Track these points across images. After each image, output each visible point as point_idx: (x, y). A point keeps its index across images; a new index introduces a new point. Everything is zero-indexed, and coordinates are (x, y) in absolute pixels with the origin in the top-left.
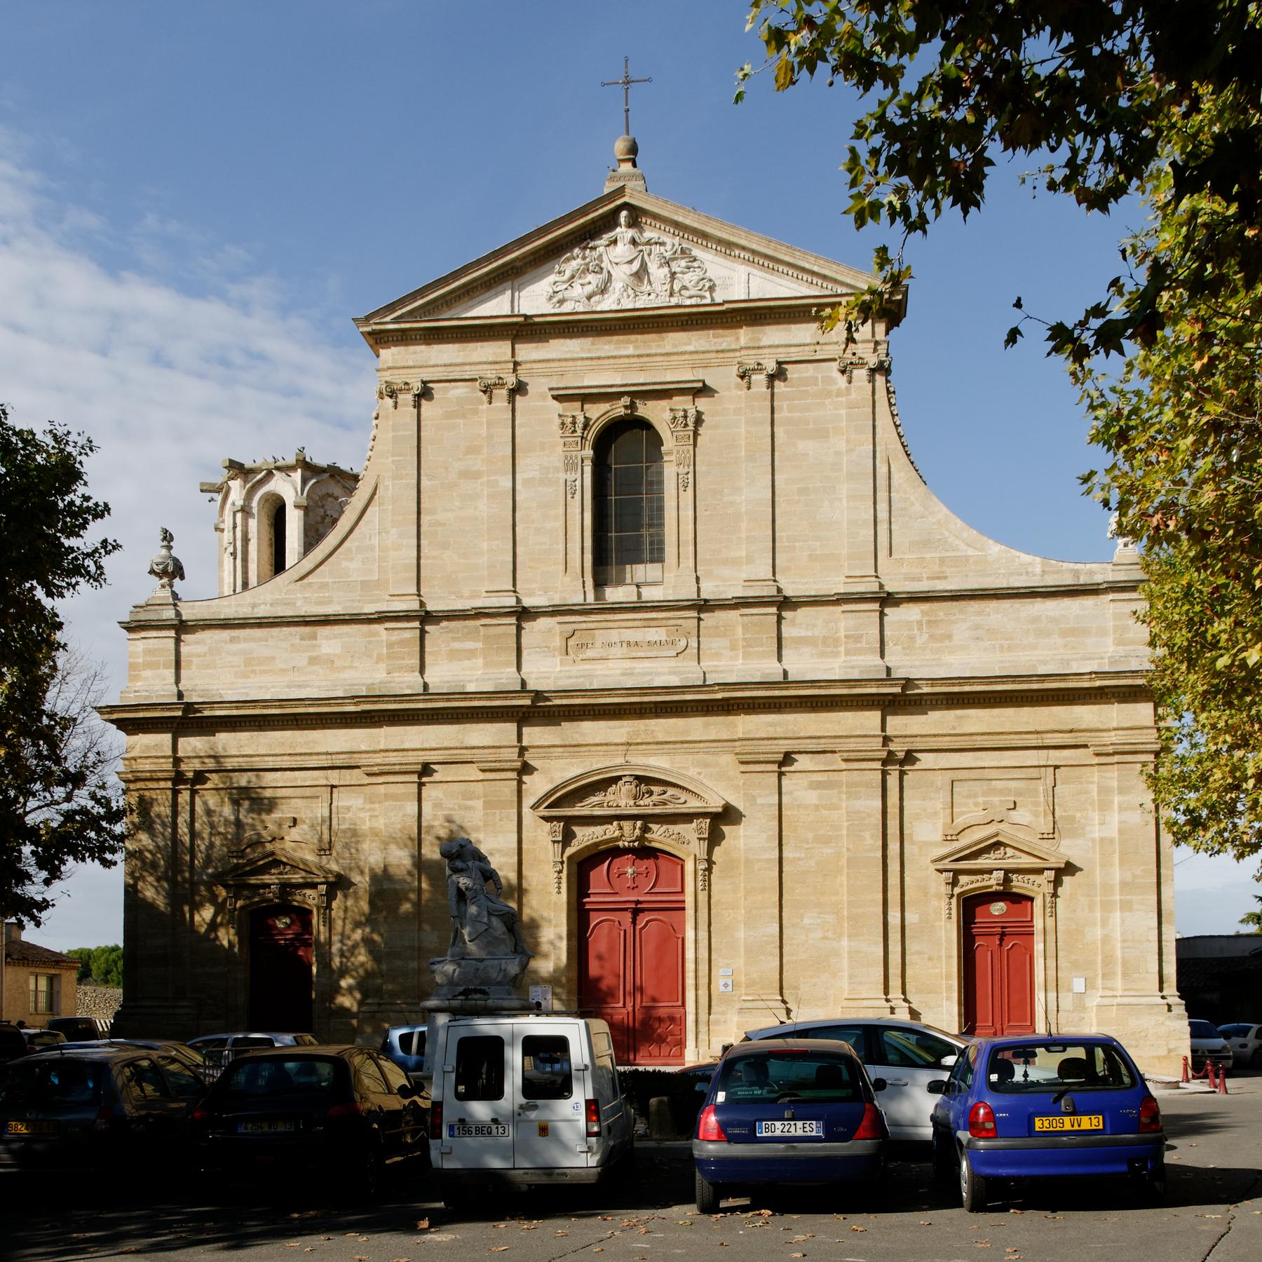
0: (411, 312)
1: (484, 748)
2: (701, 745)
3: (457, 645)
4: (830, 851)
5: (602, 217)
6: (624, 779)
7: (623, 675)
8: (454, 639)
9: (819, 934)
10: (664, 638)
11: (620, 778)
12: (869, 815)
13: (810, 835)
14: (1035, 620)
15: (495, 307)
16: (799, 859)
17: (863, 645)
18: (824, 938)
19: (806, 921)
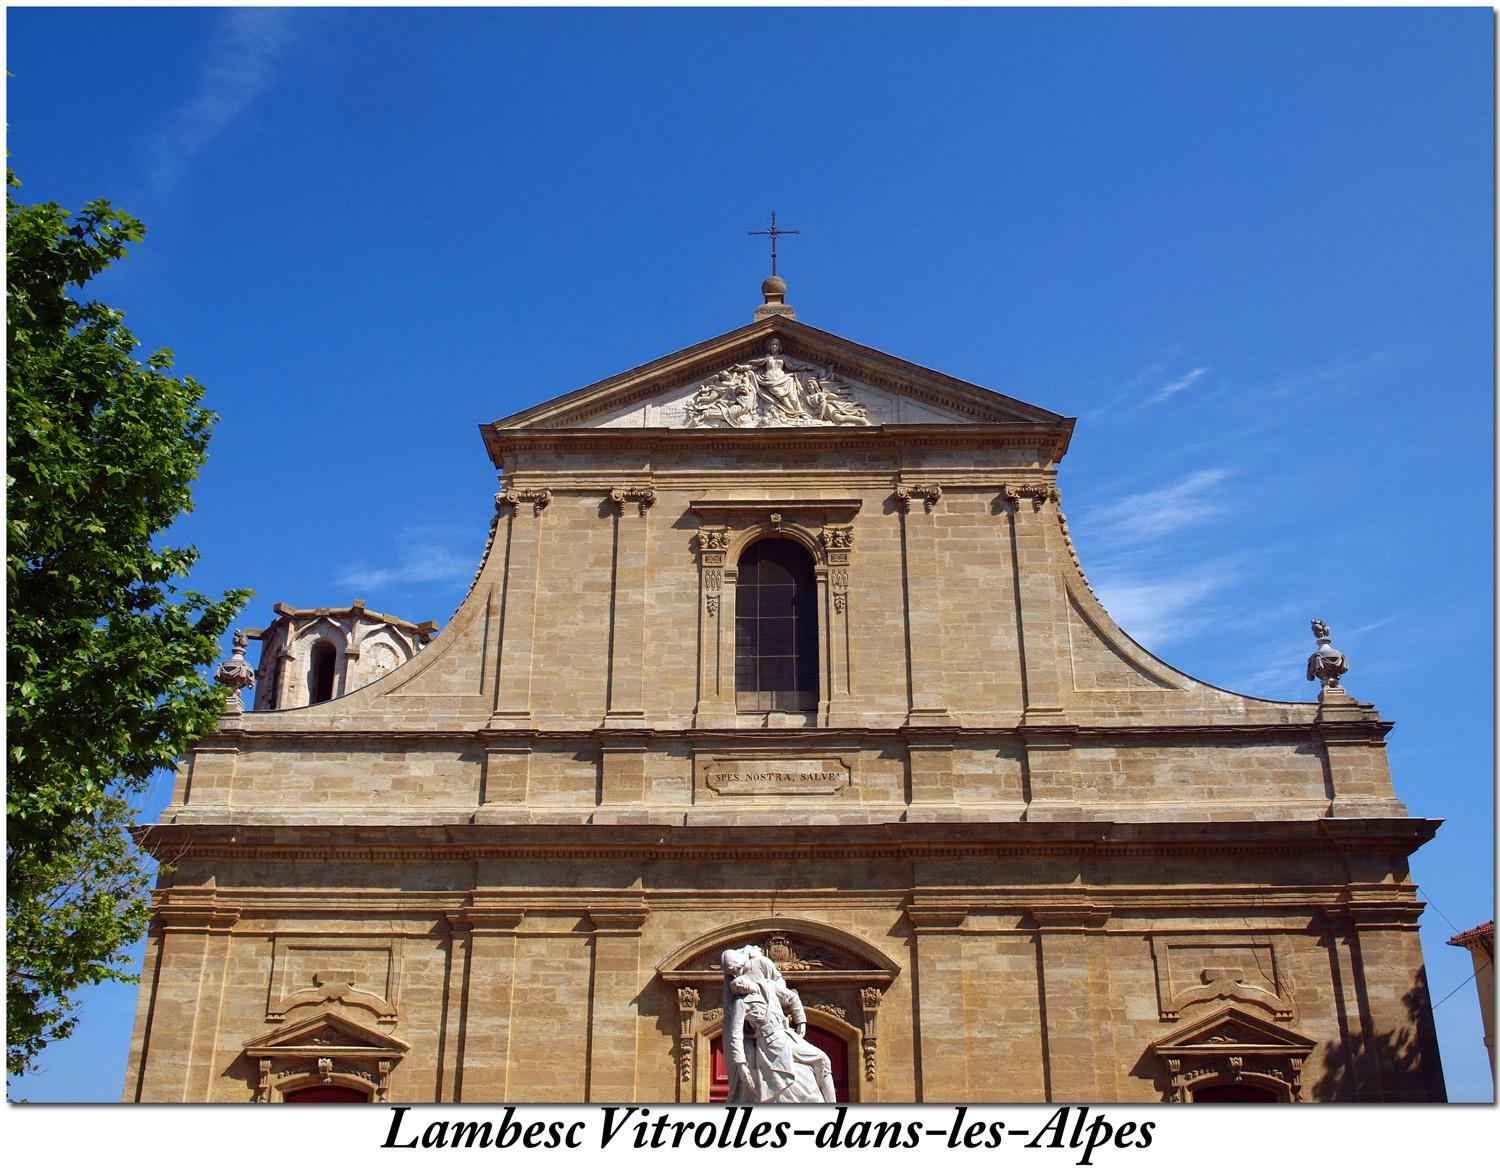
4: (1028, 1030)
8: (568, 765)
10: (820, 771)
13: (1002, 1011)
16: (990, 1040)
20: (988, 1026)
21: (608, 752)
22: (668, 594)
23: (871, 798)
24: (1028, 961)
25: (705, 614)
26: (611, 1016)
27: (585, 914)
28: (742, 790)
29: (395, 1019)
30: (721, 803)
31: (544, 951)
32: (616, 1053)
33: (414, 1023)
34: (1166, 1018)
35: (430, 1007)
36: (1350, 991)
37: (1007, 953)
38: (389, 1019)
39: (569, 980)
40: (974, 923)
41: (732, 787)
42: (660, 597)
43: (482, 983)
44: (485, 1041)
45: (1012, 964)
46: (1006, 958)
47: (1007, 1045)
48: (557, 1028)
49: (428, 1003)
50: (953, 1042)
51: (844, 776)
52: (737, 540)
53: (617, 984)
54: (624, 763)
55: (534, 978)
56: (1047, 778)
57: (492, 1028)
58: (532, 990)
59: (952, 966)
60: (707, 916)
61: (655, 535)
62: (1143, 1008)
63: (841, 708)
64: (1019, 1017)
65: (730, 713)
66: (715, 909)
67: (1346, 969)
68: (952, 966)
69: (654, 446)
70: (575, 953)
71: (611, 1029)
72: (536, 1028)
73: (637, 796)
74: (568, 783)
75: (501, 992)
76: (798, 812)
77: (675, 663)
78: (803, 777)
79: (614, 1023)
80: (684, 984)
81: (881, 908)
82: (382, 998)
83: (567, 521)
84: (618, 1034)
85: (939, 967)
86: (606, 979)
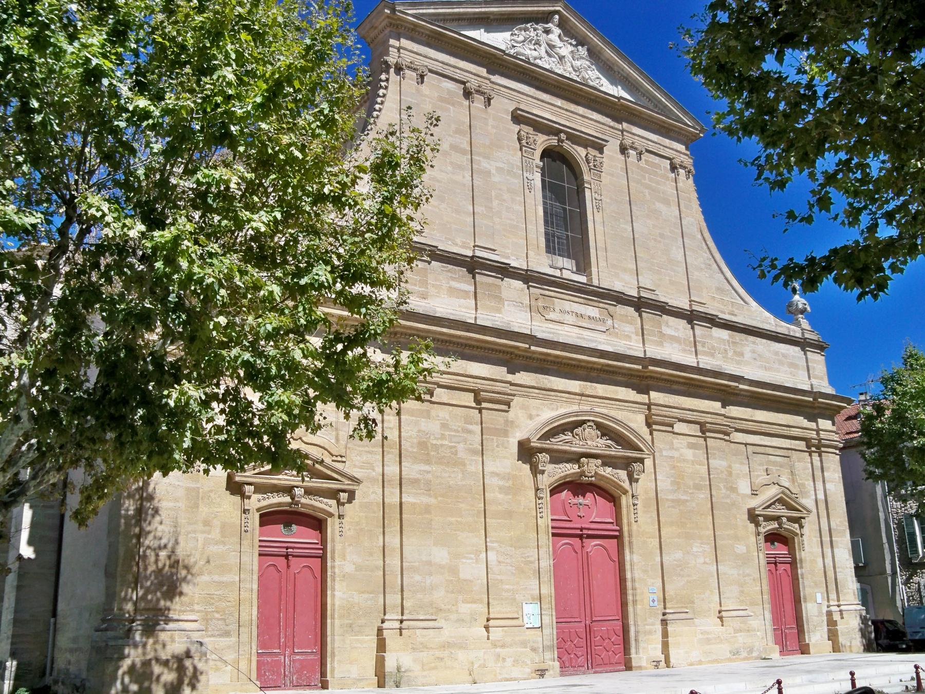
0: (423, 14)
1: (484, 379)
2: (626, 404)
3: (455, 284)
4: (702, 496)
5: (543, 12)
6: (589, 424)
7: (578, 338)
8: (453, 279)
9: (701, 560)
10: (598, 316)
11: (584, 422)
12: (722, 472)
13: (691, 483)
14: (777, 353)
15: (499, 40)
16: (687, 501)
17: (706, 349)
18: (705, 563)
19: (695, 549)
20: (685, 492)
21: (479, 273)
22: (502, 169)
23: (623, 336)
24: (701, 454)
25: (527, 191)
26: (495, 470)
27: (476, 392)
28: (557, 319)
29: (344, 459)
30: (547, 325)
31: (447, 418)
32: (501, 496)
33: (357, 463)
34: (754, 494)
35: (369, 452)
36: (820, 485)
37: (691, 448)
38: (339, 458)
39: (465, 441)
40: (679, 427)
41: (552, 316)
42: (499, 170)
43: (411, 437)
44: (415, 482)
45: (694, 456)
46: (691, 451)
47: (694, 505)
48: (460, 475)
49: (367, 449)
50: (673, 501)
51: (610, 322)
52: (542, 141)
53: (497, 446)
54: (490, 285)
55: (443, 437)
56: (703, 345)
57: (420, 472)
58: (442, 445)
59: (670, 453)
60: (543, 404)
61: (496, 121)
62: (744, 487)
63: (605, 275)
64: (698, 487)
65: (542, 263)
66: (548, 400)
67: (818, 473)
68: (670, 453)
69: (65, 21)
70: (468, 421)
71: (496, 479)
72: (447, 475)
73: (499, 310)
74: (452, 292)
75: (423, 445)
76: (592, 341)
77: (511, 220)
78: (589, 317)
79: (497, 475)
80: (541, 450)
81: (634, 412)
82: (333, 441)
83: (436, 95)
84: (501, 483)
85: (664, 453)
86: (492, 442)
